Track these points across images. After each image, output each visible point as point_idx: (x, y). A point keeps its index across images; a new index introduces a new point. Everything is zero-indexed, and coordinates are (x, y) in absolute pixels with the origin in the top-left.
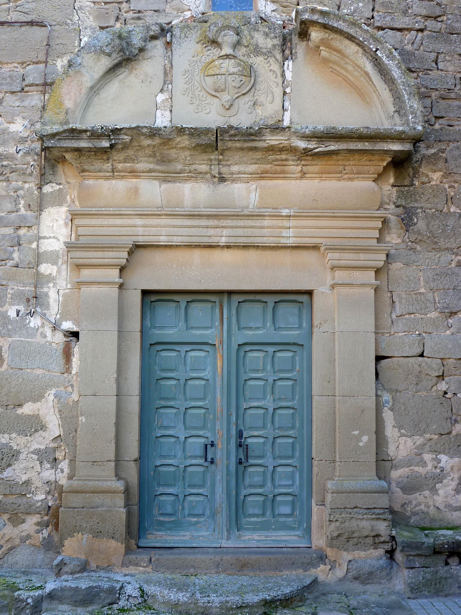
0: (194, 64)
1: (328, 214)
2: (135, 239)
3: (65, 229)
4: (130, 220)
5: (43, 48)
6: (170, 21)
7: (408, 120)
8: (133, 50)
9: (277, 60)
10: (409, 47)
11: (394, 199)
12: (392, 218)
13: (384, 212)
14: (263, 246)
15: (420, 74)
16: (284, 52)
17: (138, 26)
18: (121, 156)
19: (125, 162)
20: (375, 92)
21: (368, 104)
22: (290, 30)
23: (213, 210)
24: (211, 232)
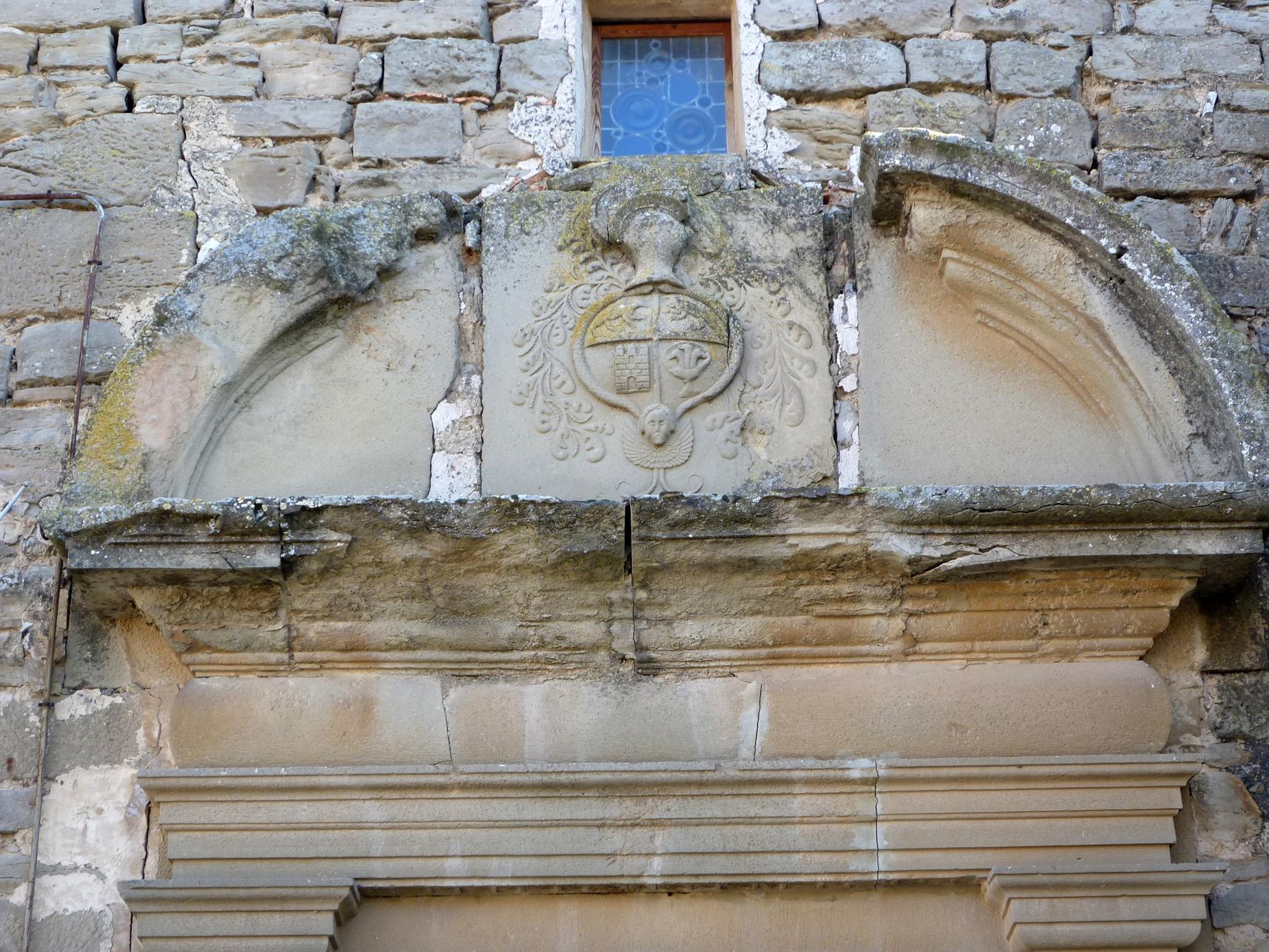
0: (550, 311)
1: (1004, 771)
2: (360, 868)
3: (124, 839)
4: (343, 805)
5: (78, 271)
6: (473, 188)
7: (1238, 461)
8: (361, 274)
9: (808, 293)
10: (1215, 247)
11: (1213, 715)
12: (1214, 777)
13: (1188, 756)
14: (788, 885)
15: (1258, 324)
16: (828, 269)
17: (375, 204)
18: (318, 597)
19: (329, 617)
20: (1124, 380)
21: (1106, 416)
22: (843, 208)
23: (620, 766)
24: (616, 840)
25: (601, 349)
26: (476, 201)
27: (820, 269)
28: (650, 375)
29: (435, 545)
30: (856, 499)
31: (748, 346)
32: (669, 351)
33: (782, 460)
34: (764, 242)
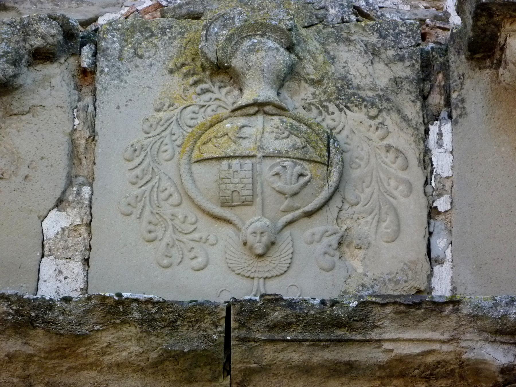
0: (160, 129)
6: (90, 16)
9: (405, 119)
25: (207, 164)
26: (92, 27)
27: (417, 97)
28: (253, 189)
29: (39, 341)
30: (451, 307)
31: (347, 166)
32: (272, 167)
33: (378, 273)
34: (364, 72)
